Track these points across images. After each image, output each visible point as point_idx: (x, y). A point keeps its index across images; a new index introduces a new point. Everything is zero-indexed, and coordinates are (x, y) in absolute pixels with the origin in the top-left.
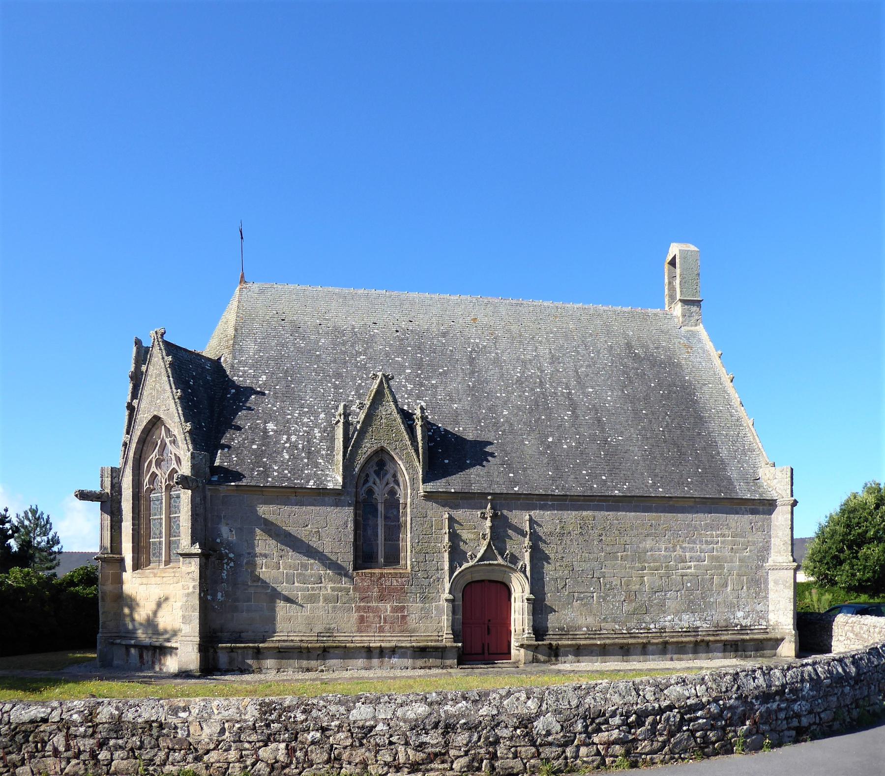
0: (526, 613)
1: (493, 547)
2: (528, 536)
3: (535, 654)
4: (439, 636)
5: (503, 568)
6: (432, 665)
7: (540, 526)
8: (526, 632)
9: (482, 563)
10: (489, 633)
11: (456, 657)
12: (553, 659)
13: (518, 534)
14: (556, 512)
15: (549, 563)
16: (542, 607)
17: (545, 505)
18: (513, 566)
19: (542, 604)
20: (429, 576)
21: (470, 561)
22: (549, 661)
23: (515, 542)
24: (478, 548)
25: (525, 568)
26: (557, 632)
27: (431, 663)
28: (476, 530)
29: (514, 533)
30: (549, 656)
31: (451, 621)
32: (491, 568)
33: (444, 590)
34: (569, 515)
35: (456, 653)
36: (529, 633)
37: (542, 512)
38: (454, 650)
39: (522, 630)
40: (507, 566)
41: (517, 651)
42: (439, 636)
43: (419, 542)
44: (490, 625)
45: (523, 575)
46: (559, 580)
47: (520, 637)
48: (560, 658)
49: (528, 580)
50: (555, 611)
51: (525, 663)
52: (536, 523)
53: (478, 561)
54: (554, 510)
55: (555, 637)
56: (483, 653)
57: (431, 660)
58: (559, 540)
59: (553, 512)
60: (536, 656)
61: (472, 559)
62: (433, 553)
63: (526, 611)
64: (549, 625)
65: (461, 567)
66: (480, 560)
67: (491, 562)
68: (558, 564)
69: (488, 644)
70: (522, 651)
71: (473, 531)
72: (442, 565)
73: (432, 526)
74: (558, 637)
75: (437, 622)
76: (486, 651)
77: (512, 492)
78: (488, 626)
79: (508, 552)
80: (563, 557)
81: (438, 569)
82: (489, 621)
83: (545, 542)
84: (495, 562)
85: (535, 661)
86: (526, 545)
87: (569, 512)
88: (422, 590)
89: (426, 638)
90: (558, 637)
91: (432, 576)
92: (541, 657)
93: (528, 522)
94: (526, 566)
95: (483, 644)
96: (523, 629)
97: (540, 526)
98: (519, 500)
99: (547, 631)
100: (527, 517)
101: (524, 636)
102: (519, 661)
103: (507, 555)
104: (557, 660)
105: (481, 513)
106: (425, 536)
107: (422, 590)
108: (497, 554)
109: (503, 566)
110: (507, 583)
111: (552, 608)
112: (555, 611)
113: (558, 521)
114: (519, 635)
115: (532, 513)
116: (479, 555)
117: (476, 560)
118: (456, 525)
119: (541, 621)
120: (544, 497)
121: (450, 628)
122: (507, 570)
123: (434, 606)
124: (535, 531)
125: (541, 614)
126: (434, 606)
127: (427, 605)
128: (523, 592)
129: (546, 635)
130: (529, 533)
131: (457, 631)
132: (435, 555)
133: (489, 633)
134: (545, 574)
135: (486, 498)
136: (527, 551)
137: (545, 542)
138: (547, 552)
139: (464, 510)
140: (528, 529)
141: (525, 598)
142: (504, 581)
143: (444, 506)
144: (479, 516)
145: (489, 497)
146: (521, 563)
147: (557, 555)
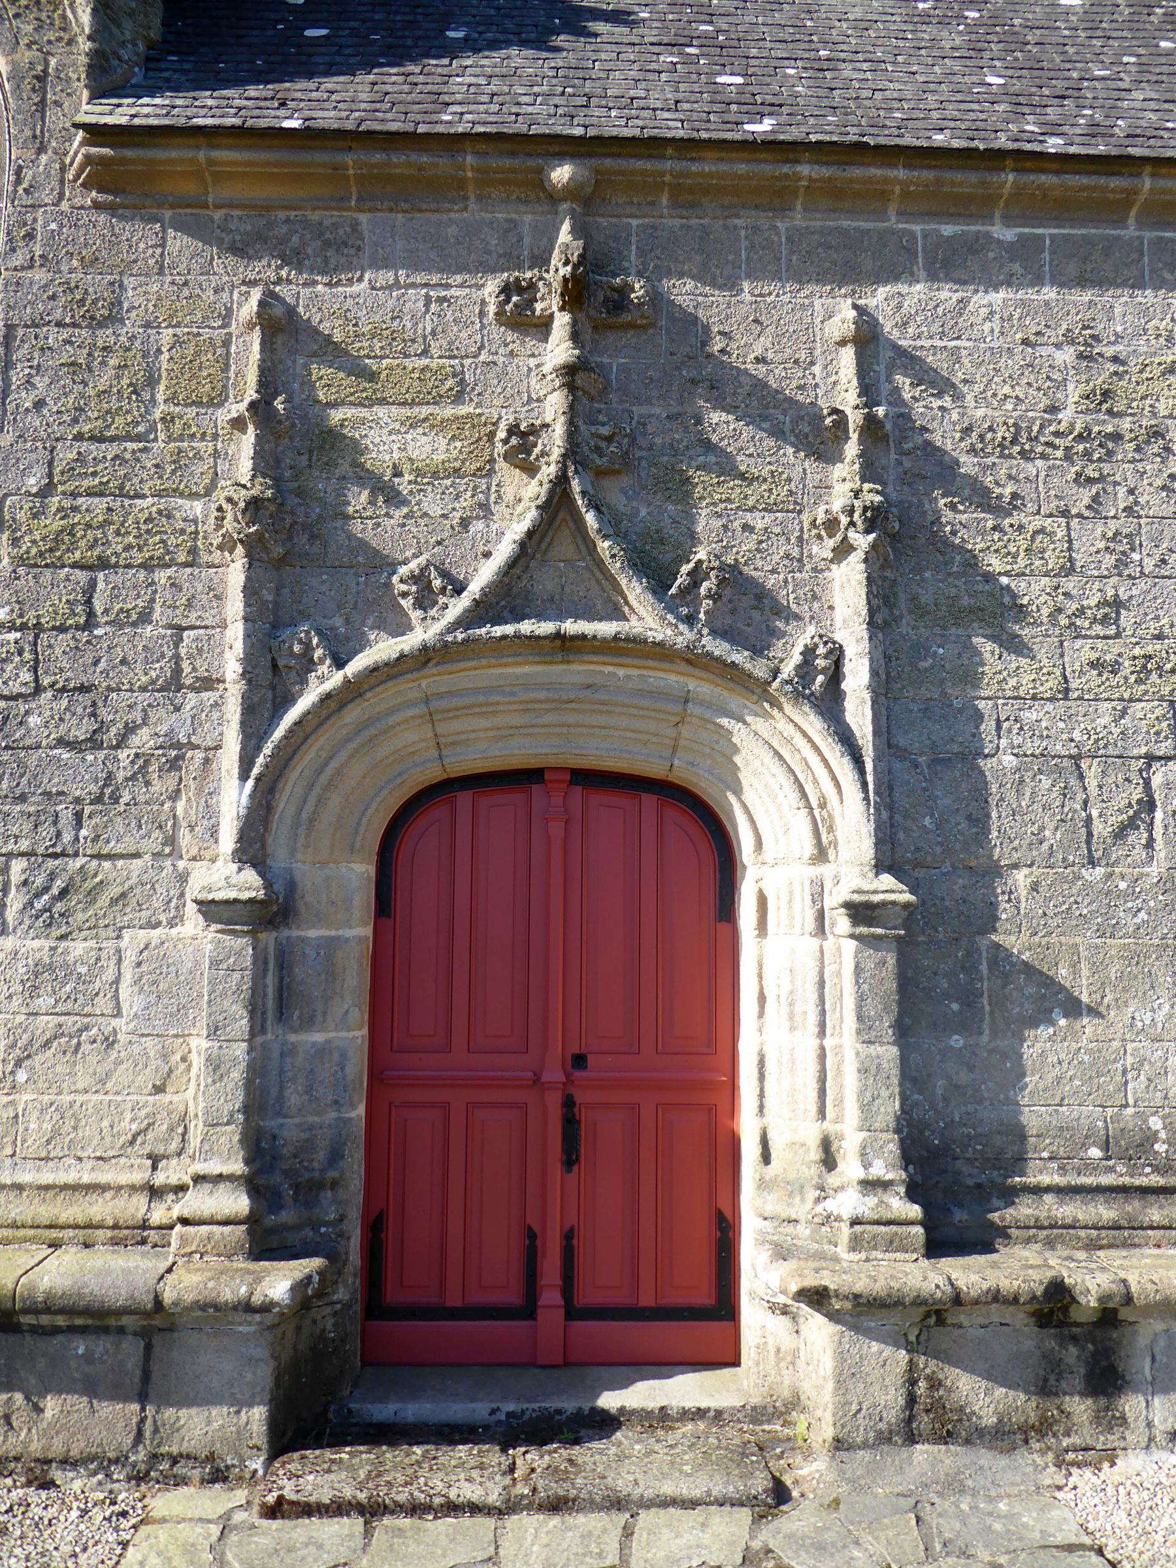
0: (850, 1022)
1: (590, 518)
2: (852, 449)
3: (928, 1365)
4: (155, 1192)
5: (672, 679)
6: (57, 1448)
7: (941, 385)
8: (850, 1169)
9: (498, 631)
10: (570, 1159)
11: (264, 1374)
12: (1080, 1407)
13: (778, 433)
14: (1049, 293)
15: (1015, 645)
16: (969, 966)
17: (975, 246)
18: (739, 657)
19: (972, 952)
20: (102, 727)
21: (415, 615)
22: (1043, 1428)
23: (754, 493)
24: (478, 526)
25: (836, 675)
26: (1088, 1167)
27: (56, 1427)
28: (463, 410)
29: (747, 432)
30: (1045, 1389)
31: (237, 1075)
32: (577, 671)
33: (214, 832)
34: (1145, 312)
35: (260, 1352)
36: (870, 1185)
37: (948, 294)
38: (247, 1327)
39: (815, 1154)
40: (693, 659)
41: (780, 1323)
42: (155, 1192)
43: (46, 491)
44: (580, 1097)
45: (814, 724)
46: (1092, 771)
47: (802, 1208)
48: (1132, 1404)
49: (861, 771)
50: (1074, 1008)
51: (840, 1444)
52: (907, 360)
53: (469, 620)
54: (1037, 281)
55: (1069, 1210)
56: (528, 1310)
57: (51, 1405)
58: (1082, 480)
59: (1030, 294)
60: (935, 1384)
61: (426, 599)
62: (147, 566)
63: (849, 1003)
64: (1034, 1117)
65: (340, 664)
66: (482, 611)
67: (571, 627)
68: (1082, 652)
69: (569, 1236)
70: (819, 1331)
71: (449, 411)
72: (210, 647)
73: (152, 381)
74: (1106, 1212)
75: (148, 1078)
76: (550, 1297)
77: (738, 136)
78: (569, 1103)
79: (702, 554)
80: (1117, 604)
81: (175, 683)
82: (580, 1061)
83: (982, 498)
84: (606, 628)
85: (924, 1422)
86: (837, 505)
87: (1148, 297)
88: (47, 831)
89: (45, 1211)
90: (1106, 1212)
91: (130, 729)
92: (869, 514)
93: (847, 357)
94: (837, 656)
95: (532, 1235)
96: (826, 1145)
97: (941, 385)
98: (784, 209)
99: (1019, 1162)
100: (844, 318)
101: (830, 1205)
102: (795, 1403)
103: (697, 577)
104: (1114, 1421)
105: (506, 290)
106: (94, 450)
107: (47, 831)
108: (615, 567)
109: (660, 652)
110: (705, 787)
111: (1050, 983)
112: (1074, 1008)
113: (1066, 356)
114: (795, 1189)
115: (878, 298)
116: (482, 576)
117: (458, 606)
118: (320, 372)
119: (964, 1078)
120: (965, 180)
121: (231, 1136)
122: (699, 686)
123: (130, 957)
124: (904, 418)
125: (967, 1024)
126: (130, 957)
127: (78, 948)
128: (821, 855)
129: (1010, 1195)
130: (855, 418)
131: (308, 1146)
132: (162, 576)
133: (570, 1159)
134: (988, 726)
135: (538, 183)
136: (843, 550)
137: (982, 498)
138: (995, 564)
139: (385, 277)
140: (848, 399)
141: (834, 898)
142: (683, 772)
143: (240, 250)
144: (492, 309)
145: (562, 174)
146: (804, 636)
147: (1070, 584)
